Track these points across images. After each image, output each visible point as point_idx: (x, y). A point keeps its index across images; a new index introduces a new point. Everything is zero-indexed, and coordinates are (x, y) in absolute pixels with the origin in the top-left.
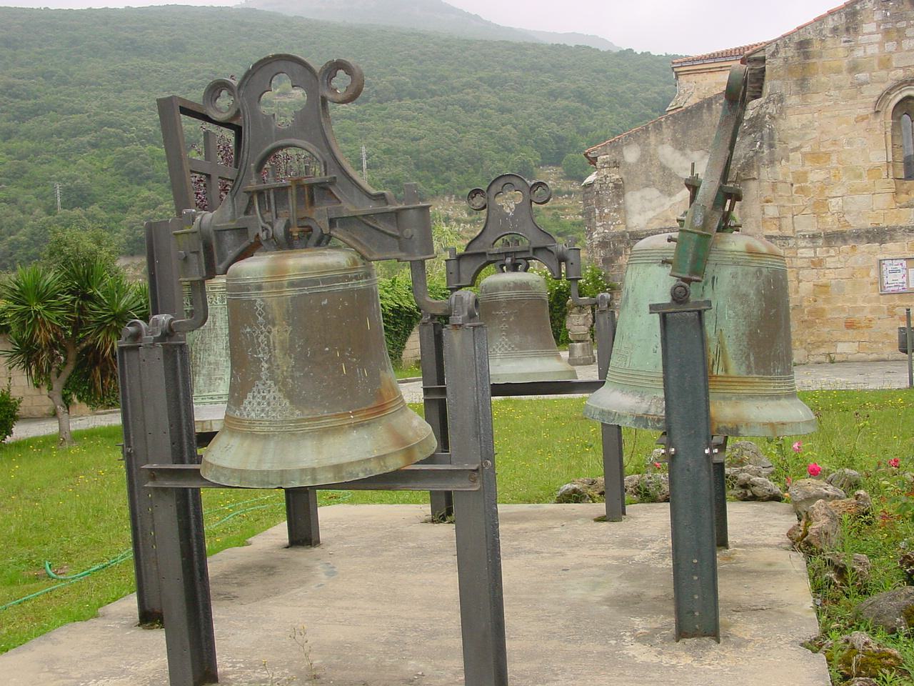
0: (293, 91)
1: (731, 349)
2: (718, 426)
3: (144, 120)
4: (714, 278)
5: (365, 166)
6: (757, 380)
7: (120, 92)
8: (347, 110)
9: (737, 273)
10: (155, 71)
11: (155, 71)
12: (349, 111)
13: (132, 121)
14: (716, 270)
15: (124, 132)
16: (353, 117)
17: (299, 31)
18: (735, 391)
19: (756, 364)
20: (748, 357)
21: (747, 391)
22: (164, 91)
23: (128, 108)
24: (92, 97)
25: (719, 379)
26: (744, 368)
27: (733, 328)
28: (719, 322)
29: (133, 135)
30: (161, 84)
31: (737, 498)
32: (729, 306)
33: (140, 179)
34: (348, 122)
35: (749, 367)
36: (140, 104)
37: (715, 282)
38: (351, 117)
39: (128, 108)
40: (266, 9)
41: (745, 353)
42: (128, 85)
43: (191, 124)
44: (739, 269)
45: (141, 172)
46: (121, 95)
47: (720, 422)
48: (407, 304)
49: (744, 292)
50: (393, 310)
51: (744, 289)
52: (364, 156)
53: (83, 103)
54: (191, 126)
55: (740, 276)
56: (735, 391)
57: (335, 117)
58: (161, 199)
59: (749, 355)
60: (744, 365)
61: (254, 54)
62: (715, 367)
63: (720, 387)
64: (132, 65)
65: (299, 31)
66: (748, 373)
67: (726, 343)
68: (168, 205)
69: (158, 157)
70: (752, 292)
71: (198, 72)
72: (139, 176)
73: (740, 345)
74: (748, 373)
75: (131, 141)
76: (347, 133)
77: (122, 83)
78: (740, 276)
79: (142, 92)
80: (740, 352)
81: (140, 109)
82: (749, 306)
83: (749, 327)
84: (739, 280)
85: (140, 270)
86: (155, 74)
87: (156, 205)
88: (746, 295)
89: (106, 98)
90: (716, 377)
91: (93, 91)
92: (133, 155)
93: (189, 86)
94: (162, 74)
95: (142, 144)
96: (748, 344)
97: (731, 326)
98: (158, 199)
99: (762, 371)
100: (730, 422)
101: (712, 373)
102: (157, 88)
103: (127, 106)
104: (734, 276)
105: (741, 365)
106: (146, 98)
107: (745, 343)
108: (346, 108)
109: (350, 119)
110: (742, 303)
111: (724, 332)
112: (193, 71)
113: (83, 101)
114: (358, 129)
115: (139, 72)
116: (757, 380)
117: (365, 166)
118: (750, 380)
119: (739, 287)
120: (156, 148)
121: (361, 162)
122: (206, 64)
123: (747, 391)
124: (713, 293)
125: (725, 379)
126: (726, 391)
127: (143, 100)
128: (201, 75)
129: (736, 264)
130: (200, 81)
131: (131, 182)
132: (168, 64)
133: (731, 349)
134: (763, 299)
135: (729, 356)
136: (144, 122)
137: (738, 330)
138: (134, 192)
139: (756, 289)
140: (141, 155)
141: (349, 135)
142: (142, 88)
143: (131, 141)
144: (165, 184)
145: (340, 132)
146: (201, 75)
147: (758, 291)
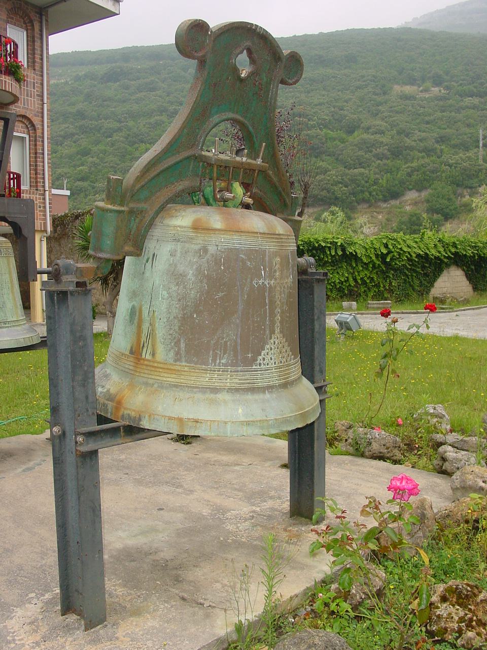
0: (433, 89)
1: (161, 332)
2: (124, 413)
3: (323, 112)
4: (154, 255)
5: (481, 145)
6: (186, 369)
7: (309, 92)
8: (472, 102)
9: (176, 251)
10: (333, 77)
11: (333, 77)
12: (473, 103)
13: (314, 113)
14: (157, 247)
15: (309, 120)
16: (476, 107)
17: (441, 43)
18: (158, 378)
19: (188, 352)
20: (177, 343)
21: (173, 380)
22: (339, 91)
23: (313, 104)
24: (290, 97)
25: (146, 363)
26: (172, 354)
27: (165, 310)
28: (153, 303)
29: (315, 122)
30: (337, 86)
31: (435, 469)
32: (164, 286)
33: (317, 153)
34: (472, 111)
35: (177, 353)
36: (321, 101)
37: (155, 259)
38: (474, 107)
39: (313, 104)
40: (419, 27)
41: (175, 338)
42: (314, 87)
43: (356, 114)
44: (179, 246)
45: (318, 148)
46: (309, 95)
47: (125, 409)
48: (433, 252)
49: (181, 272)
50: (418, 256)
51: (181, 268)
52: (481, 137)
53: (283, 101)
54: (355, 116)
55: (178, 254)
56: (158, 378)
57: (461, 108)
58: (330, 167)
59: (179, 341)
60: (172, 351)
61: (406, 62)
62: (145, 350)
63: (146, 372)
64: (318, 73)
65: (441, 43)
66: (176, 361)
67: (157, 325)
68: (334, 172)
69: (330, 138)
70: (190, 274)
71: (363, 77)
72: (317, 151)
73: (171, 329)
74: (176, 361)
75: (313, 127)
76: (470, 120)
77: (311, 86)
78: (178, 254)
79: (323, 93)
80: (170, 337)
81: (320, 104)
82: (185, 287)
83: (183, 310)
84: (178, 258)
85: (313, 217)
86: (333, 79)
87: (326, 171)
88: (183, 275)
89: (298, 97)
90: (144, 360)
91: (291, 92)
92: (313, 137)
93: (356, 87)
94: (339, 79)
95: (321, 129)
96: (180, 329)
97: (164, 307)
98: (328, 168)
99: (195, 359)
100: (134, 411)
101: (141, 356)
102: (334, 89)
103: (313, 103)
104: (173, 254)
105: (170, 350)
106: (326, 96)
107: (177, 328)
108: (471, 100)
109: (474, 109)
110: (177, 284)
111: (156, 314)
112: (359, 76)
113: (283, 100)
114: (479, 116)
115: (323, 78)
116: (186, 369)
117: (481, 145)
118: (179, 368)
119: (176, 266)
120: (329, 131)
121: (479, 141)
122: (370, 71)
123: (173, 380)
124: (152, 272)
125: (151, 364)
126: (150, 376)
127: (324, 98)
128: (365, 79)
129: (177, 240)
130: (364, 83)
131: (310, 156)
132: (343, 72)
133: (161, 332)
134: (205, 281)
135: (158, 340)
136: (322, 113)
137: (170, 313)
138: (312, 162)
139: (197, 268)
140: (319, 137)
141: (472, 121)
142: (324, 89)
143: (313, 127)
144: (333, 157)
145: (465, 119)
146: (365, 79)
147: (199, 271)
